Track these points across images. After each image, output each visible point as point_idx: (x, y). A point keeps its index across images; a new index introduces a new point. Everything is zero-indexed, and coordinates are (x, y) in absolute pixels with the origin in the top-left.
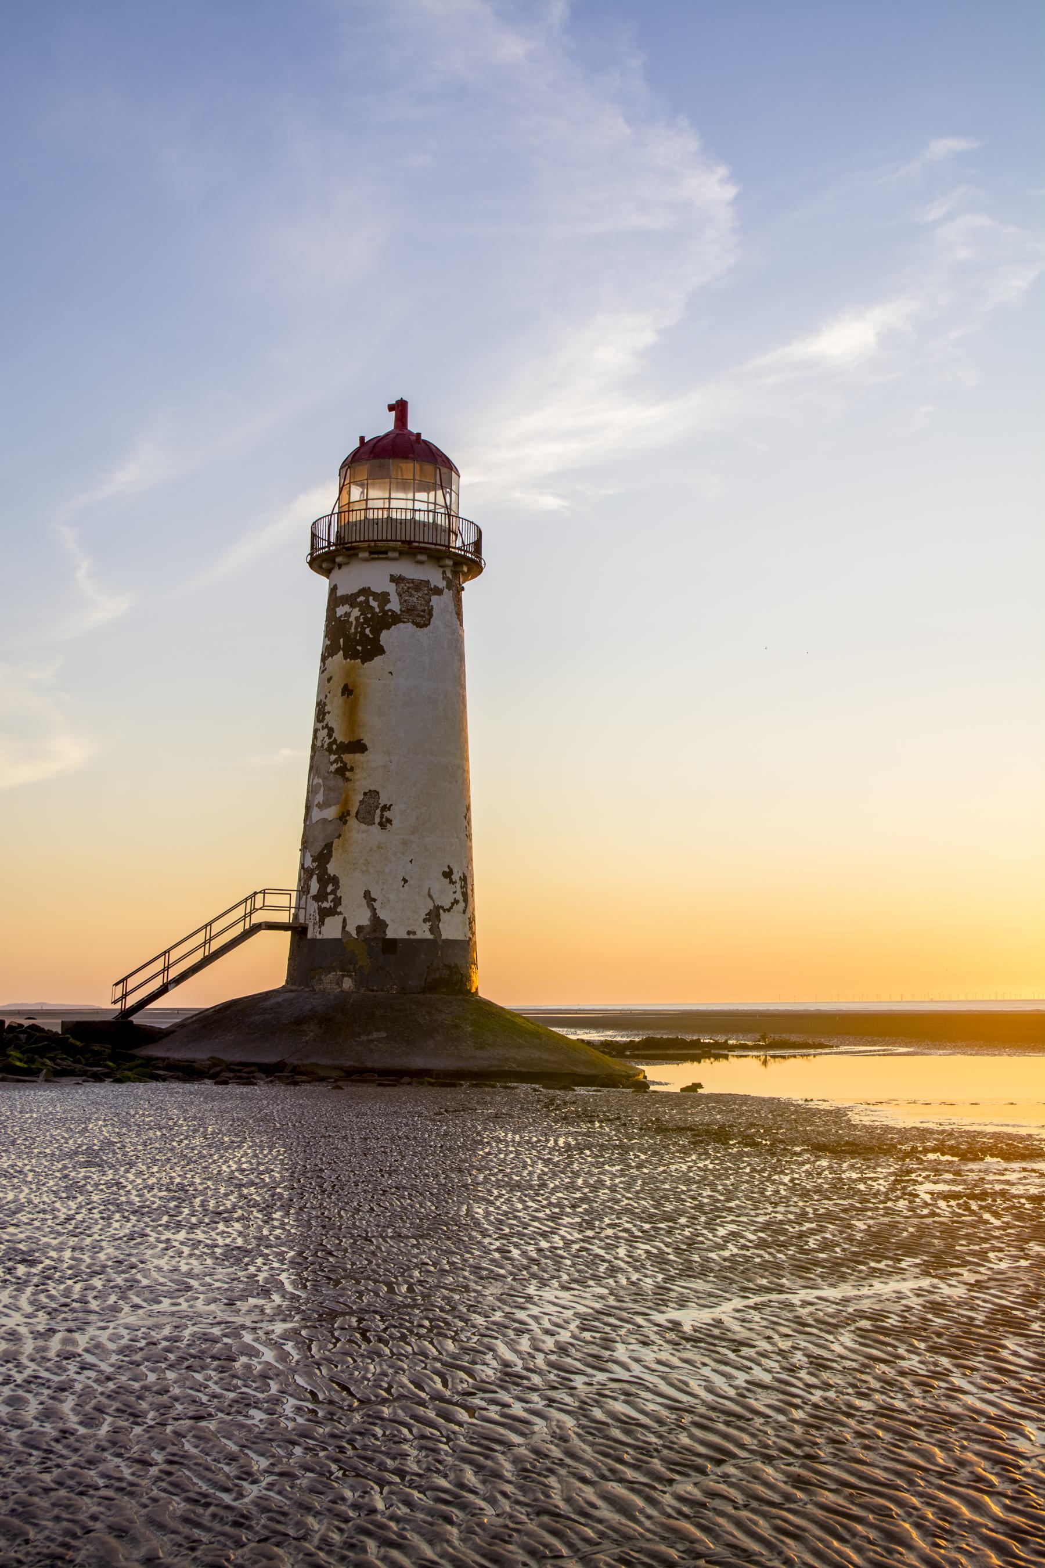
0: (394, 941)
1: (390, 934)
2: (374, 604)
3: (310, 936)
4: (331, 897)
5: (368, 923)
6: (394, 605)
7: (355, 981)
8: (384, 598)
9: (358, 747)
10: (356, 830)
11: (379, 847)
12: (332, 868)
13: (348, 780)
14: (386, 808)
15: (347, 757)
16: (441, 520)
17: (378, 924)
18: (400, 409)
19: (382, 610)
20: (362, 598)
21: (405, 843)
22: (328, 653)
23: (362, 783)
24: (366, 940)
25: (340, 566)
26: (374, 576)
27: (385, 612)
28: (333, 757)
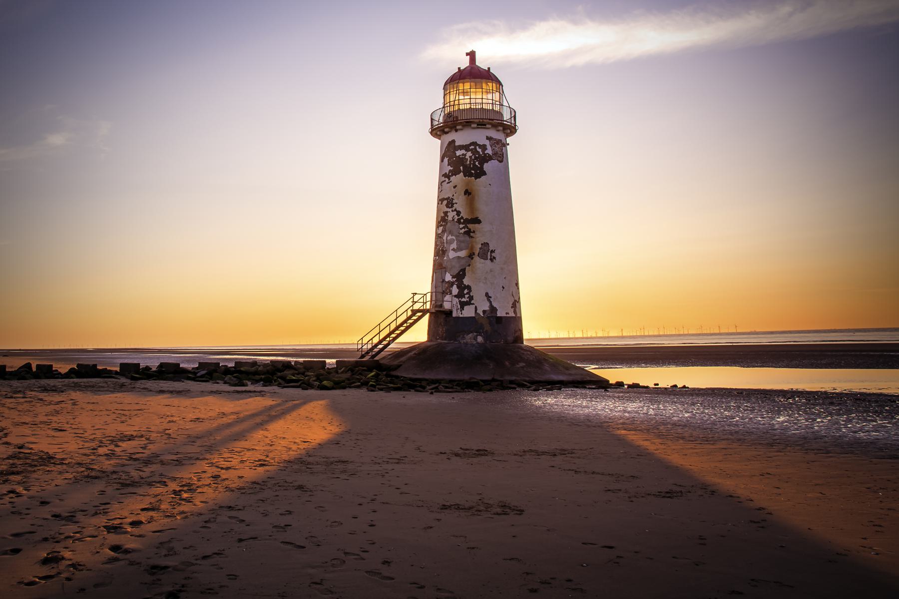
0: (501, 317)
1: (499, 315)
2: (479, 150)
4: (467, 296)
6: (489, 151)
7: (484, 338)
8: (484, 147)
9: (477, 221)
10: (478, 262)
11: (491, 271)
12: (466, 281)
14: (492, 251)
16: (497, 108)
17: (493, 309)
19: (484, 153)
20: (472, 147)
21: (502, 269)
22: (445, 176)
23: (479, 239)
24: (488, 317)
26: (462, 137)
27: (485, 154)
28: (461, 226)
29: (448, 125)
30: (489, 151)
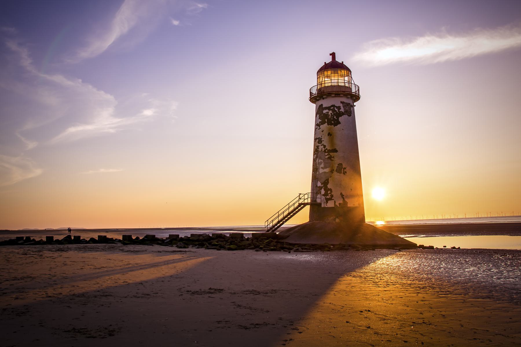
3: (323, 206)
4: (330, 195)
5: (18, 176)
6: (342, 110)
8: (339, 108)
10: (336, 175)
13: (332, 160)
14: (344, 168)
15: (331, 154)
16: (347, 85)
18: (333, 55)
19: (339, 111)
22: (317, 125)
25: (323, 99)
26: (326, 103)
28: (326, 154)
29: (319, 96)
30: (342, 110)
